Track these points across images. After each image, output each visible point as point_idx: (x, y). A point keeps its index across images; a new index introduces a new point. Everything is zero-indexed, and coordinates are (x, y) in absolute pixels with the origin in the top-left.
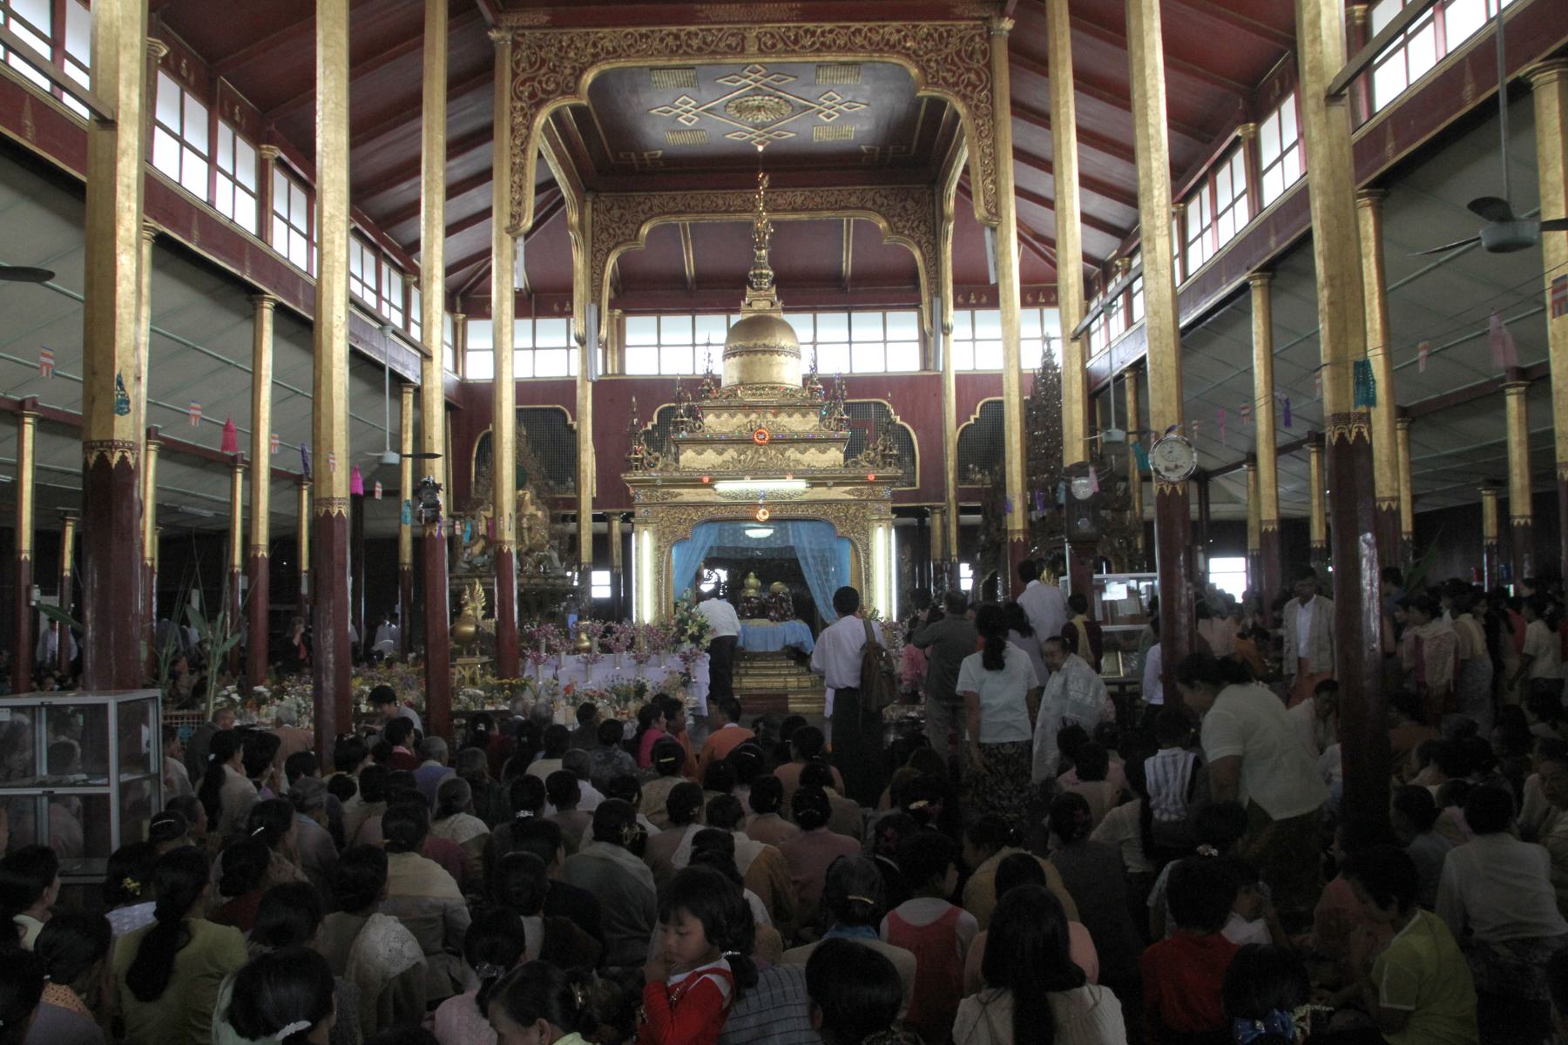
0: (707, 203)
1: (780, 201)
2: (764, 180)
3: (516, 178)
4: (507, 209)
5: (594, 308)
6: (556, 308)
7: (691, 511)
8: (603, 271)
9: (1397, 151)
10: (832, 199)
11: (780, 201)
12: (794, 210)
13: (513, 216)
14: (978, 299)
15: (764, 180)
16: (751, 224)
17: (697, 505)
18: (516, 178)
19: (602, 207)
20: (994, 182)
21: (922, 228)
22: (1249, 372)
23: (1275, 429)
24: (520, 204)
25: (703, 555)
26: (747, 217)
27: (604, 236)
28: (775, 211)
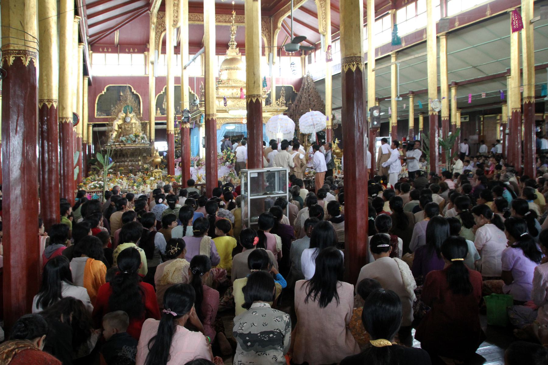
0: (196, 18)
1: (221, 19)
2: (234, 13)
3: (175, 8)
4: (172, 19)
5: (157, 51)
6: (127, 50)
7: (221, 120)
8: (159, 39)
9: (459, 25)
10: (238, 19)
11: (221, 19)
12: (226, 22)
13: (174, 21)
14: (108, 49)
15: (234, 13)
16: (229, 27)
17: (223, 118)
18: (175, 8)
19: (160, 17)
20: (325, 21)
21: (267, 30)
22: (390, 81)
23: (333, 103)
24: (177, 17)
25: (224, 134)
26: (228, 24)
27: (160, 27)
28: (219, 22)
